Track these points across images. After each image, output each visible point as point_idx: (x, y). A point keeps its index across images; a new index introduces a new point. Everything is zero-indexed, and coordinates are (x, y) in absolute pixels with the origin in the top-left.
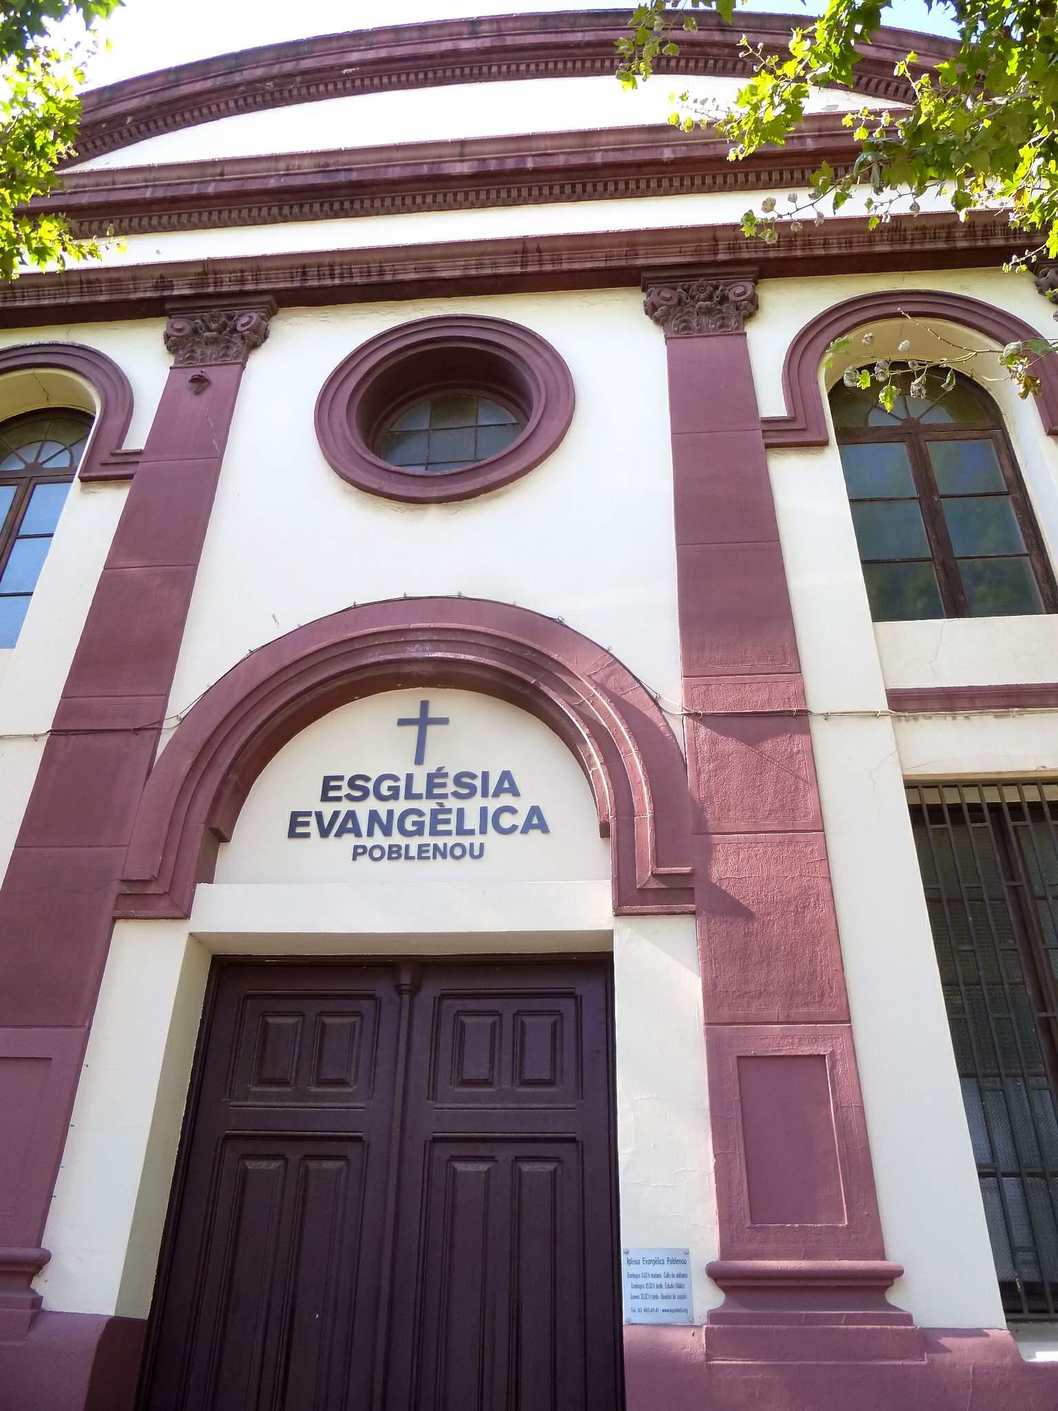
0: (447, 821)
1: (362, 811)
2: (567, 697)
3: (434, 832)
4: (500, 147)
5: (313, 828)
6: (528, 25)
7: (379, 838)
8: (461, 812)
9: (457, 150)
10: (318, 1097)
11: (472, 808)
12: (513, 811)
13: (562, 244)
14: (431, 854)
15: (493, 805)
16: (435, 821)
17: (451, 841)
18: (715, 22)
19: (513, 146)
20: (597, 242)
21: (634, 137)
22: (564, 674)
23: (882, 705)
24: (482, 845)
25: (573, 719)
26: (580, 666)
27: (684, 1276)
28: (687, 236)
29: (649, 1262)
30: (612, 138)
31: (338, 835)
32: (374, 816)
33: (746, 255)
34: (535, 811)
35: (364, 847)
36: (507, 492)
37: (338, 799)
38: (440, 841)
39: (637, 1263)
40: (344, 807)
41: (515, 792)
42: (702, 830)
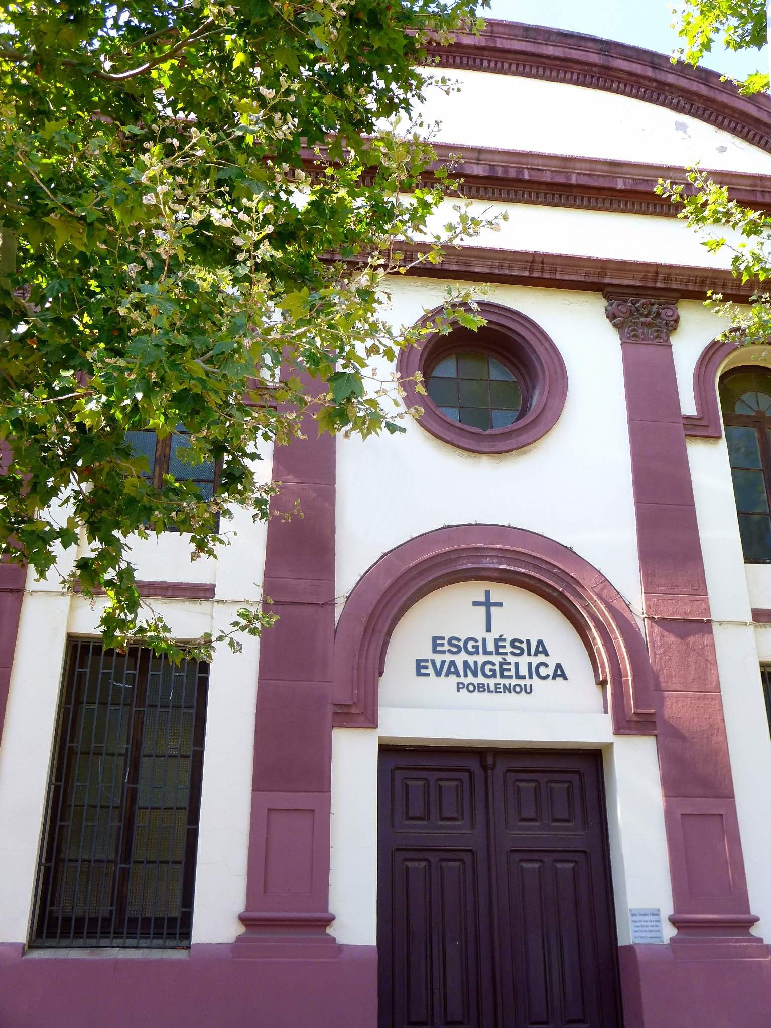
0: (510, 670)
1: (460, 659)
2: (580, 601)
3: (502, 676)
4: (505, 158)
5: (430, 670)
6: (514, 32)
7: (470, 678)
8: (517, 664)
9: (475, 155)
10: (443, 827)
11: (523, 660)
12: (546, 665)
13: (558, 261)
14: (502, 690)
15: (535, 661)
16: (502, 670)
17: (514, 682)
18: (649, 60)
19: (515, 159)
20: (582, 263)
21: (600, 167)
22: (577, 585)
23: (749, 618)
24: (531, 686)
25: (585, 616)
26: (587, 581)
27: (659, 921)
28: (640, 268)
29: (642, 915)
30: (584, 165)
31: (447, 675)
32: (466, 663)
33: (674, 286)
34: (558, 666)
35: (463, 683)
36: (530, 451)
37: (443, 652)
38: (507, 682)
39: (636, 915)
40: (448, 657)
41: (547, 654)
42: (658, 688)
